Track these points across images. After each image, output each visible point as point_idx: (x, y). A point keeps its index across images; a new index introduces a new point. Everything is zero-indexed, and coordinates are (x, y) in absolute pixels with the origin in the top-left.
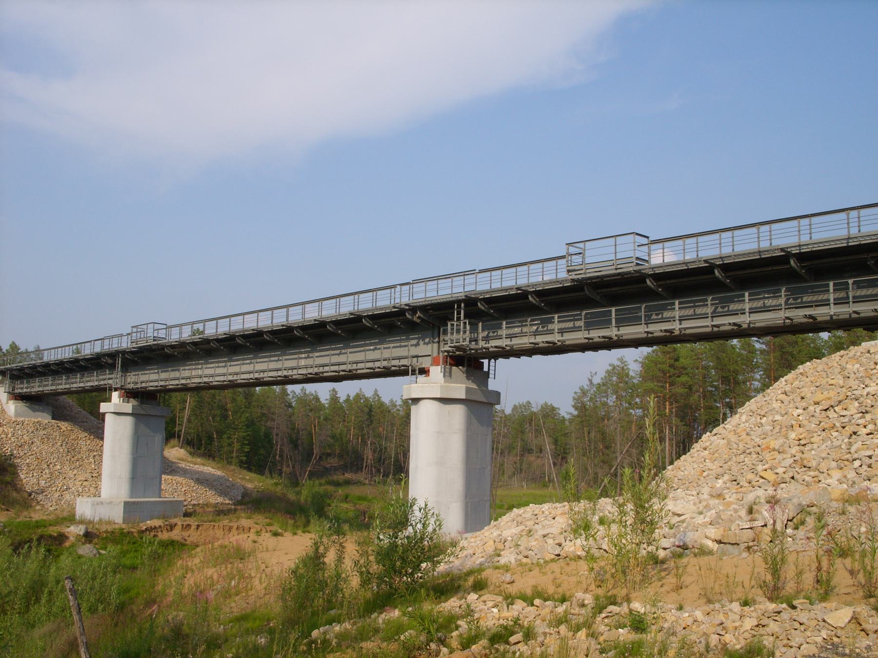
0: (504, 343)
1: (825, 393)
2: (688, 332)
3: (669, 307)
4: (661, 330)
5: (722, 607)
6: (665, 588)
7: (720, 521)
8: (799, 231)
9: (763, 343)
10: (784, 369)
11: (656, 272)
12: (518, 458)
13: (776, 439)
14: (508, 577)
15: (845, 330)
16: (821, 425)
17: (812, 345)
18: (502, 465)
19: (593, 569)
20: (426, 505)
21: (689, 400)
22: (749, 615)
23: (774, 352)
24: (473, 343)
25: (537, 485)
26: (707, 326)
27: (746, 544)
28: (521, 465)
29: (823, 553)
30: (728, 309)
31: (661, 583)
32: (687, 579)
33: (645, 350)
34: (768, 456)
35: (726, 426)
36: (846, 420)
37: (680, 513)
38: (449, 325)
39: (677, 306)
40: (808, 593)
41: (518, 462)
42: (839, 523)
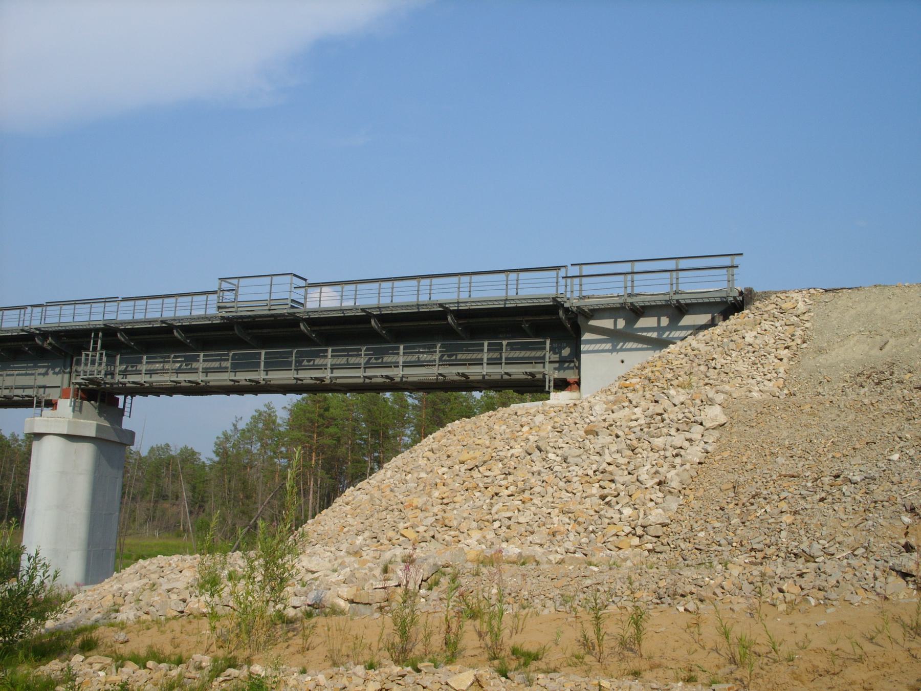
0: (142, 379)
1: (471, 452)
2: (339, 381)
3: (321, 354)
4: (311, 378)
5: (347, 671)
6: (291, 649)
7: (354, 580)
8: (459, 288)
9: (416, 398)
10: (435, 426)
11: (311, 317)
12: (152, 504)
13: (419, 497)
14: (122, 636)
15: (496, 391)
16: (464, 485)
17: (464, 404)
18: (134, 511)
19: (215, 628)
20: (37, 554)
21: (337, 452)
22: (373, 678)
23: (426, 408)
24: (109, 377)
25: (171, 535)
26: (359, 377)
27: (378, 604)
28: (154, 512)
29: (454, 614)
30: (314, 363)
31: (287, 644)
32: (314, 640)
33: (294, 398)
34: (410, 514)
35: (370, 481)
36: (489, 480)
37: (314, 569)
38: (83, 355)
39: (329, 354)
40: (435, 655)
41: (151, 509)
42: (472, 584)
